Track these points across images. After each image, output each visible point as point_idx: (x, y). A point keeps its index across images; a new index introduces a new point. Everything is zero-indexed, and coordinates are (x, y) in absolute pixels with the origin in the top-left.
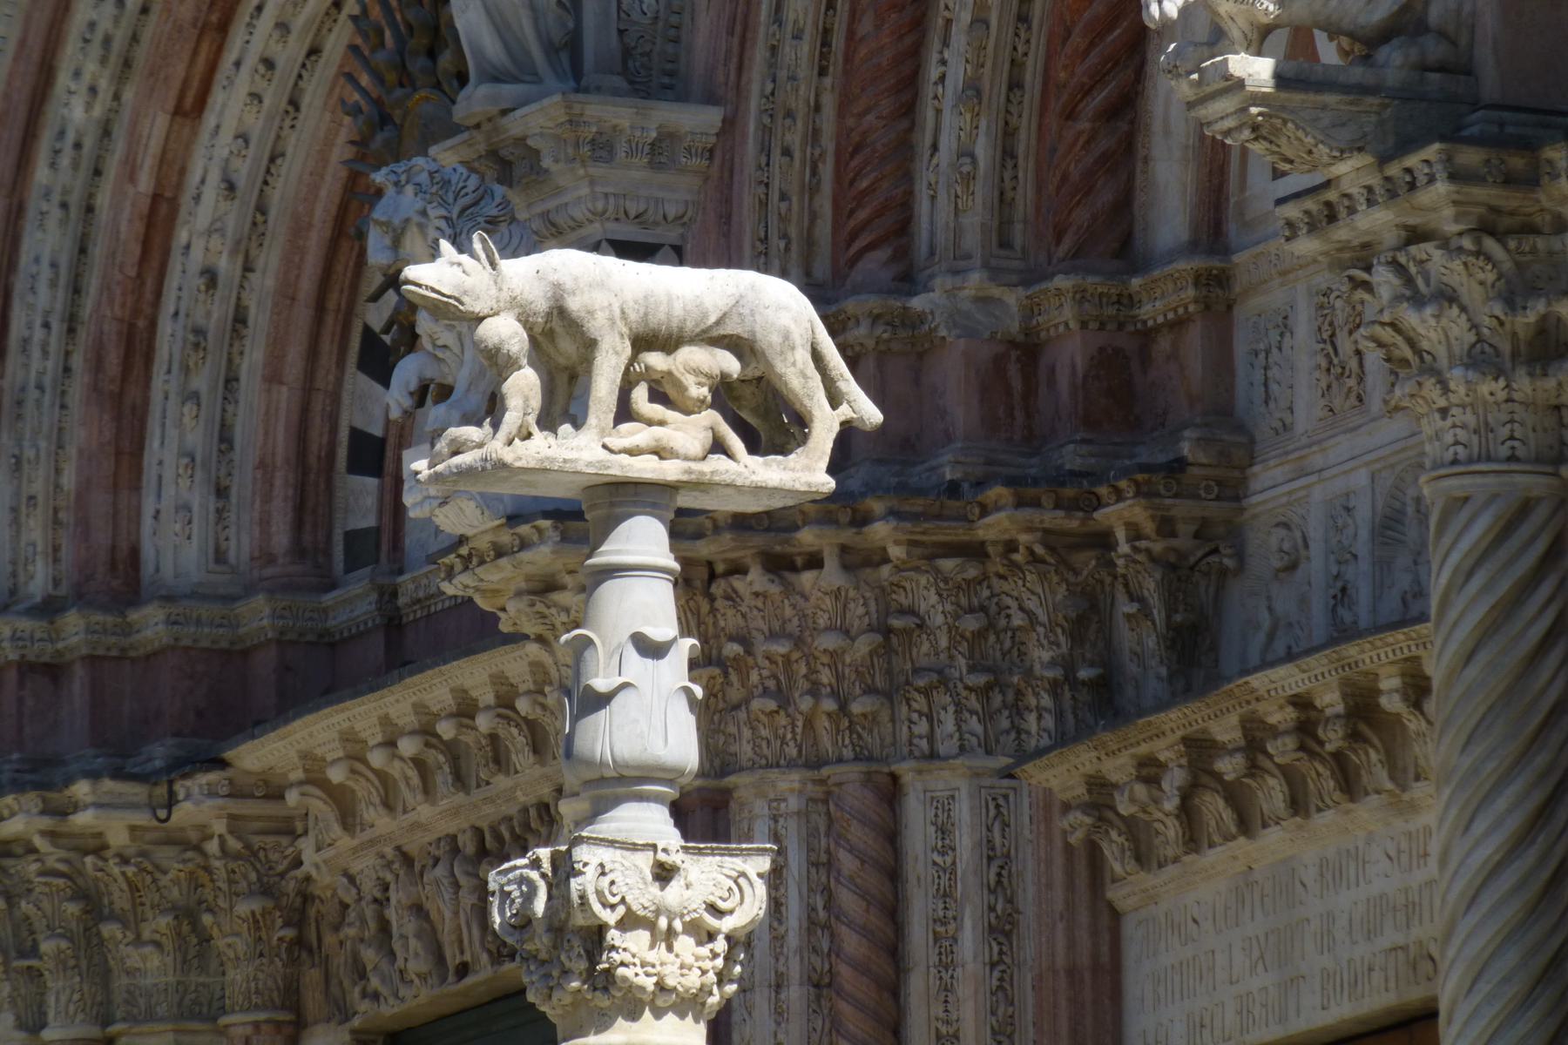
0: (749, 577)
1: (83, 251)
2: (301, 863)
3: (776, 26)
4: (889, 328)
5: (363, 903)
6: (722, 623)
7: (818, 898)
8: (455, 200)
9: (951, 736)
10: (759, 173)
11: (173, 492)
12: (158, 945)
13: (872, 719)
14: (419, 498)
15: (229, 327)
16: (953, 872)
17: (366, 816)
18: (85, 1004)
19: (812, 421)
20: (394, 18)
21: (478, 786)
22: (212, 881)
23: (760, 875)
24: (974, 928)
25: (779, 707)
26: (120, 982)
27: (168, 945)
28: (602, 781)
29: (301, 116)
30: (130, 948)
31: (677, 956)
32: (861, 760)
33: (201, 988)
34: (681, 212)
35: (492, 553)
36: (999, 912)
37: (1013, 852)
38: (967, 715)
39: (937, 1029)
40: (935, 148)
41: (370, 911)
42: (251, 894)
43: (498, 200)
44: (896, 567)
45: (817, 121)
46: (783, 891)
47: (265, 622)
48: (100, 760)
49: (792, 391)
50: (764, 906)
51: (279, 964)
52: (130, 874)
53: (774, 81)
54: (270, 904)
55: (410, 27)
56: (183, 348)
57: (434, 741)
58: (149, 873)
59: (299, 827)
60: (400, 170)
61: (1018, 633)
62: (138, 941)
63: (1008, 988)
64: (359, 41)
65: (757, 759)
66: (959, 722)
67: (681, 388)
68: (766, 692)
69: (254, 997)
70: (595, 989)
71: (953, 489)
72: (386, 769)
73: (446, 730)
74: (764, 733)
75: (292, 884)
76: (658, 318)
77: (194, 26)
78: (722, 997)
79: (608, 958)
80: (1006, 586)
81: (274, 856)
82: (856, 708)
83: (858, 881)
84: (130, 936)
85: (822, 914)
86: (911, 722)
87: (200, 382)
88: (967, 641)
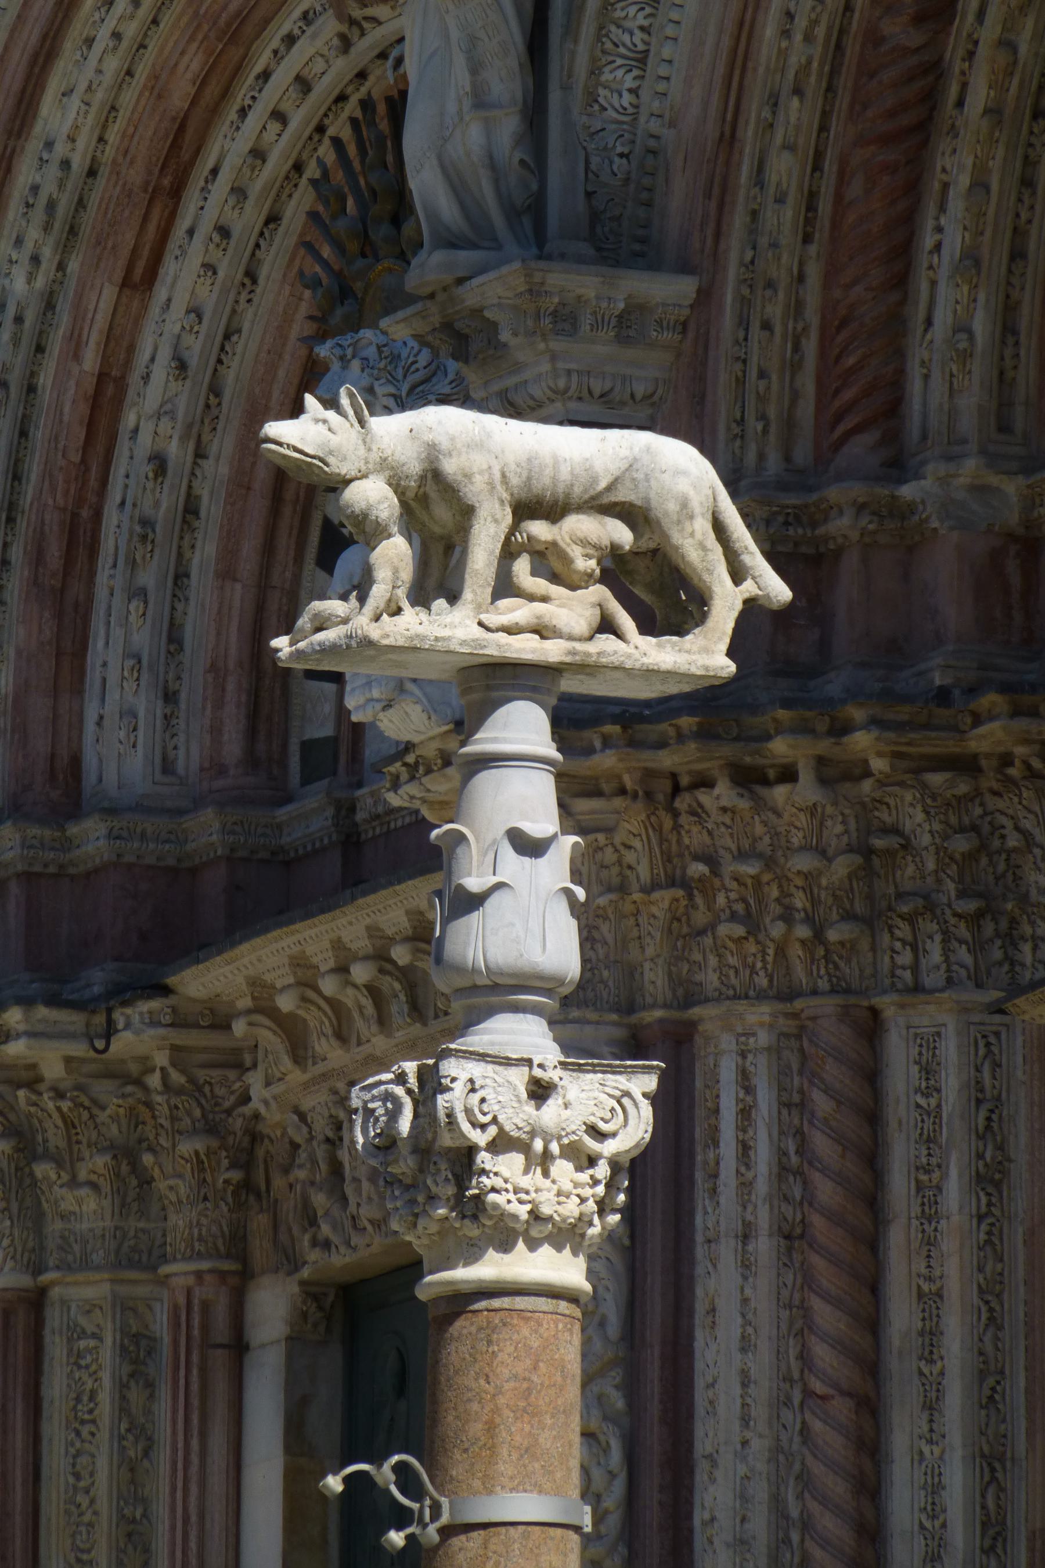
0: (717, 791)
1: (23, 434)
2: (249, 1099)
3: (757, 189)
4: (875, 518)
5: (315, 1143)
6: (687, 841)
7: (790, 1141)
8: (405, 376)
9: (938, 968)
10: (737, 348)
11: (117, 697)
12: (94, 1186)
13: (850, 947)
14: (362, 700)
15: (179, 519)
16: (938, 1115)
17: (317, 1048)
18: (15, 1250)
19: (711, 598)
20: (357, 182)
21: (436, 1017)
22: (154, 1117)
23: (645, 1095)
24: (960, 1176)
25: (748, 933)
26: (54, 1227)
27: (106, 1188)
28: (475, 989)
29: (259, 290)
30: (64, 1190)
31: (554, 1182)
32: (838, 992)
33: (140, 1235)
34: (650, 391)
35: (439, 761)
36: (988, 1159)
37: (1004, 1095)
38: (956, 944)
39: (919, 1286)
40: (929, 322)
41: (321, 1152)
42: (195, 1132)
43: (451, 376)
44: (878, 781)
45: (801, 292)
46: (751, 1133)
47: (215, 837)
48: (34, 985)
49: (689, 564)
50: (650, 1129)
51: (225, 1209)
52: (65, 1109)
53: (754, 248)
54: (215, 1144)
55: (374, 193)
56: (130, 541)
57: (388, 967)
58: (85, 1108)
59: (248, 1059)
60: (345, 343)
61: (1013, 856)
62: (73, 1183)
63: (997, 1242)
64: (321, 208)
65: (724, 989)
66: (946, 952)
67: (567, 560)
68: (733, 917)
69: (196, 1244)
70: (464, 1217)
71: (943, 696)
72: (339, 997)
73: (401, 955)
74: (732, 961)
75: (239, 1122)
76: (543, 483)
77: (145, 191)
78: (603, 1228)
79: (479, 1183)
80: (1001, 804)
81: (220, 1091)
82: (833, 935)
83: (833, 1123)
84: (65, 1177)
85: (794, 1160)
86: (893, 951)
87: (147, 578)
88: (956, 863)
